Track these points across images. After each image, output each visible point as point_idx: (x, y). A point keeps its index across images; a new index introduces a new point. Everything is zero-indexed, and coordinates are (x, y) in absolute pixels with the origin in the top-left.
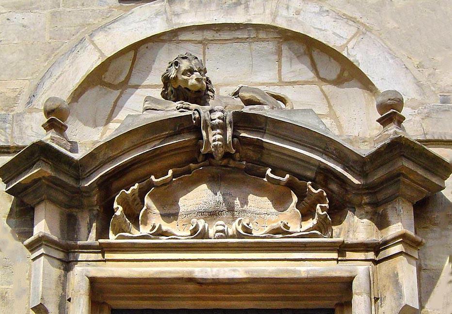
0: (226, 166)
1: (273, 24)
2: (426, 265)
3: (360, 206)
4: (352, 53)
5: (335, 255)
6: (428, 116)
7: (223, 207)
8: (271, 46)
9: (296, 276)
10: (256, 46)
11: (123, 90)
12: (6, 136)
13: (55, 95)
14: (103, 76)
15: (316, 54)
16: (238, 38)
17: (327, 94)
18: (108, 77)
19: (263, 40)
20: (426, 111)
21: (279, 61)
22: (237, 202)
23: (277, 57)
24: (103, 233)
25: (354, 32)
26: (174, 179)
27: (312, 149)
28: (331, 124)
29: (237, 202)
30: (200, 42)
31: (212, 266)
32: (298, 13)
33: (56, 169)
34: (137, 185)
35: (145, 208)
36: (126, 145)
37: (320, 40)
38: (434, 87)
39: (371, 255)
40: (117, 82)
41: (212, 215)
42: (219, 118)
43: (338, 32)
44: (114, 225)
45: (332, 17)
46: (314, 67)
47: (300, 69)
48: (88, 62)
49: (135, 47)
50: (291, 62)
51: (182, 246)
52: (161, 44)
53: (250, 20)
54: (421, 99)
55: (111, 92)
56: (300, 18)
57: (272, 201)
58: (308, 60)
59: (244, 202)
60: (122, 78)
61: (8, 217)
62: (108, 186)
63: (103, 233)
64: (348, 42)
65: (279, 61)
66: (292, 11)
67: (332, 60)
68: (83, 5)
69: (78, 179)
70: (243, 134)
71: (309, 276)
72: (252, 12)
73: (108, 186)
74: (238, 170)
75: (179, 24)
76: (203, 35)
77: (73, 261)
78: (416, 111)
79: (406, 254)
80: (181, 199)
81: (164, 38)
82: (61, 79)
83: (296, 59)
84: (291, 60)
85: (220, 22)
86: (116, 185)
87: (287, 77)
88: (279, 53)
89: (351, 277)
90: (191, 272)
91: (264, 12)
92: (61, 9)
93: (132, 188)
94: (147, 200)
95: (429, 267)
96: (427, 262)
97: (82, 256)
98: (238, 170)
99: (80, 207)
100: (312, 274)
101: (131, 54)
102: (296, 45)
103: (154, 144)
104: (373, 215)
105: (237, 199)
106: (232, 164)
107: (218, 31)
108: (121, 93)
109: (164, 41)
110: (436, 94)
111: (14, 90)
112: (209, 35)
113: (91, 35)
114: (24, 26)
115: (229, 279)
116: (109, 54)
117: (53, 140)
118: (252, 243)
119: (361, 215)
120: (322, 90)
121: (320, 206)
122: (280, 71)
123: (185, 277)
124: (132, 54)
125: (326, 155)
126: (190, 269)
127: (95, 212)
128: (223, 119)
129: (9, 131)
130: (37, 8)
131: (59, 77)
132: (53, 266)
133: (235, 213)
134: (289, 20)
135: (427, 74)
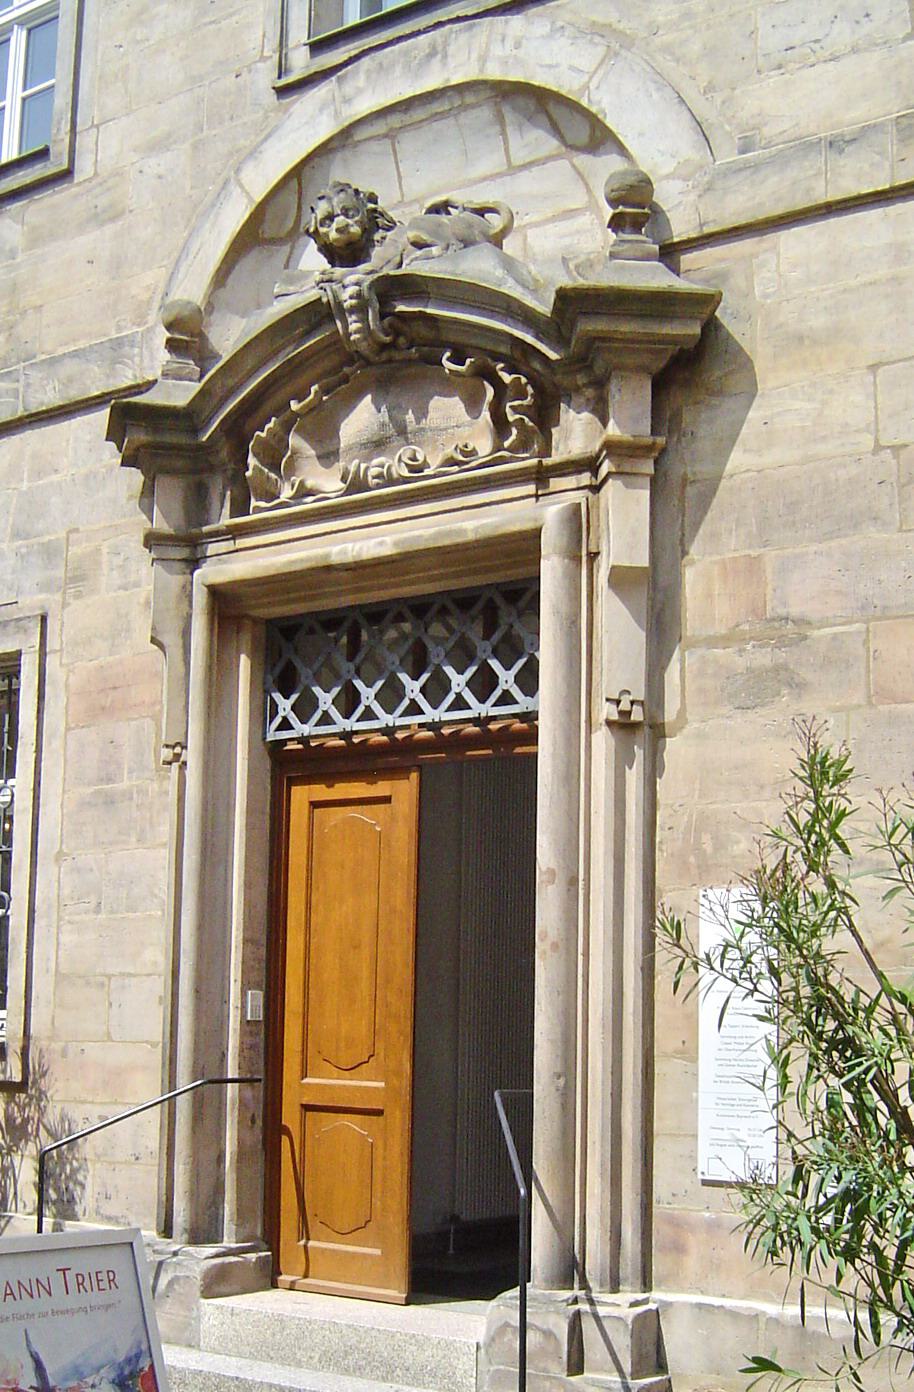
0: (390, 361)
1: (481, 77)
2: (694, 474)
3: (578, 389)
4: (595, 97)
5: (531, 489)
6: (709, 188)
7: (391, 431)
8: (485, 113)
9: (459, 540)
10: (466, 118)
11: (294, 243)
12: (135, 370)
13: (119, 329)
14: (260, 232)
15: (552, 107)
16: (437, 114)
17: (581, 170)
18: (269, 230)
19: (472, 106)
20: (706, 179)
21: (503, 133)
22: (410, 417)
23: (498, 128)
24: (240, 508)
25: (603, 53)
26: (325, 398)
27: (492, 315)
28: (592, 224)
29: (410, 417)
30: (386, 136)
31: (369, 537)
32: (518, 45)
33: (156, 430)
34: (273, 419)
35: (289, 453)
36: (250, 363)
37: (548, 87)
38: (730, 125)
39: (586, 478)
40: (283, 233)
41: (378, 445)
42: (351, 298)
43: (576, 63)
44: (255, 490)
45: (568, 38)
46: (556, 130)
47: (536, 139)
48: (234, 217)
49: (297, 173)
50: (521, 130)
51: (326, 510)
52: (331, 156)
53: (448, 80)
54: (699, 157)
55: (278, 251)
56: (521, 53)
57: (464, 402)
58: (543, 119)
59: (422, 414)
60: (290, 224)
61: (141, 497)
62: (237, 431)
63: (240, 508)
64: (591, 78)
65: (503, 133)
66: (509, 43)
67: (574, 114)
68: (232, 118)
69: (196, 431)
70: (401, 308)
71: (478, 536)
72: (452, 62)
73: (237, 431)
74: (409, 362)
75: (351, 116)
76: (387, 124)
77: (201, 558)
78: (690, 183)
79: (619, 474)
80: (343, 425)
81: (334, 144)
82: (199, 257)
83: (528, 123)
84: (520, 126)
85: (407, 96)
86: (250, 424)
87: (519, 156)
88: (500, 120)
89: (536, 529)
90: (328, 556)
91: (469, 58)
92: (205, 133)
93: (267, 427)
94: (294, 440)
95: (699, 477)
96: (697, 468)
97: (212, 549)
98: (409, 362)
99: (212, 469)
100: (483, 534)
101: (294, 184)
102: (521, 101)
103: (287, 351)
104: (597, 403)
105: (410, 412)
106: (397, 355)
107: (406, 111)
108: (292, 248)
109: (332, 151)
110: (732, 138)
111: (148, 288)
112: (395, 121)
113: (238, 171)
114: (160, 177)
115: (374, 559)
116: (259, 198)
117: (167, 375)
118: (413, 490)
119: (580, 406)
120: (574, 166)
121: (511, 407)
122: (507, 150)
123: (319, 565)
124: (294, 184)
125: (512, 317)
126: (320, 551)
127: (230, 473)
128: (359, 296)
129: (137, 359)
130: (175, 142)
131: (197, 254)
132: (171, 573)
133: (409, 436)
134: (504, 62)
135: (719, 101)
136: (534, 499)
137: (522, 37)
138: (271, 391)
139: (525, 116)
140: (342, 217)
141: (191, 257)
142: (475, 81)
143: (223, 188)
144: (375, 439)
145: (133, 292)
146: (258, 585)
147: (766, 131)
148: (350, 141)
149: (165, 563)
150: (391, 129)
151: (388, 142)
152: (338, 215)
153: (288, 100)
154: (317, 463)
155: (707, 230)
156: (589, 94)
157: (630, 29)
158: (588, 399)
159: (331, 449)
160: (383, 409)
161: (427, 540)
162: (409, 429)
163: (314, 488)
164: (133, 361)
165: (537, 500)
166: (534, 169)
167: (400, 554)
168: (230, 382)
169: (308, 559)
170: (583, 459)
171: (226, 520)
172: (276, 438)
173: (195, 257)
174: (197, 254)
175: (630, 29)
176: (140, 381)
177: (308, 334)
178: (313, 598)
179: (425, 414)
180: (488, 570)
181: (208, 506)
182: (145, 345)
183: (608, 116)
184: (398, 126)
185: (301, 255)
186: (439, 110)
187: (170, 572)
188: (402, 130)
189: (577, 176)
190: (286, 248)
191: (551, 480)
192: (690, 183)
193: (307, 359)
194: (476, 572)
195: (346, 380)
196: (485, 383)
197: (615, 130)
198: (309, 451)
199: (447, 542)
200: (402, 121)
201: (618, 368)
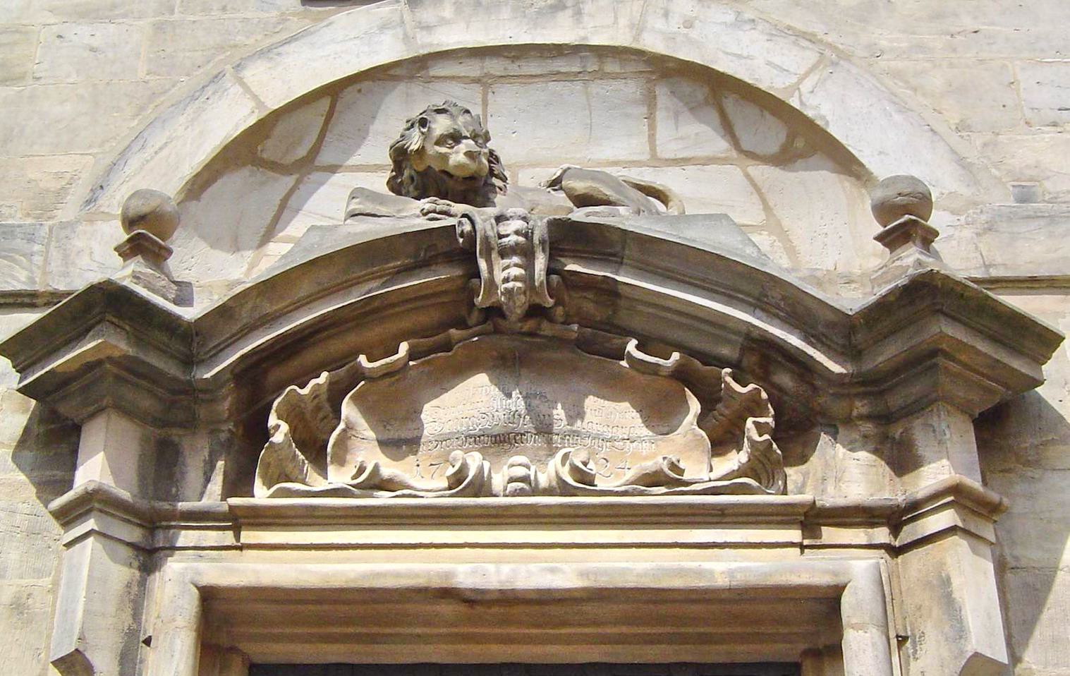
2: (1016, 558)
3: (848, 421)
5: (795, 535)
8: (632, 89)
9: (702, 583)
12: (32, 272)
14: (259, 148)
15: (730, 104)
16: (559, 73)
18: (269, 150)
19: (615, 77)
20: (984, 217)
21: (651, 117)
22: (559, 412)
24: (239, 483)
29: (559, 412)
30: (477, 81)
33: (138, 340)
34: (325, 375)
35: (342, 426)
36: (305, 288)
38: (999, 169)
40: (289, 159)
42: (517, 233)
44: (267, 466)
46: (728, 129)
47: (697, 134)
49: (334, 91)
53: (585, 38)
56: (694, 34)
57: (640, 411)
58: (714, 115)
59: (576, 413)
60: (302, 152)
63: (239, 483)
65: (651, 117)
68: (224, 9)
69: (189, 362)
74: (560, 342)
75: (431, 45)
76: (483, 68)
78: (962, 218)
81: (398, 71)
84: (676, 115)
86: (275, 375)
88: (650, 101)
90: (448, 575)
92: (177, 16)
93: (313, 382)
94: (348, 409)
95: (1023, 563)
97: (186, 538)
99: (190, 424)
100: (740, 580)
101: (325, 104)
102: (686, 87)
105: (559, 406)
106: (547, 329)
107: (514, 59)
108: (298, 182)
112: (495, 66)
113: (238, 67)
114: (93, 50)
117: (138, 278)
120: (747, 176)
121: (754, 422)
124: (325, 104)
127: (223, 436)
129: (38, 259)
130: (125, 16)
131: (161, 149)
133: (555, 437)
134: (671, 38)
135: (979, 143)
136: (798, 550)
137: (696, 18)
138: (319, 336)
139: (686, 104)
140: (471, 142)
141: (150, 151)
142: (625, 48)
143: (212, 81)
144: (496, 431)
145: (32, 176)
146: (979, 514)
147: (1048, 185)
148: (423, 73)
149: (108, 542)
150: (486, 75)
151: (477, 88)
152: (466, 138)
153: (319, 9)
154: (378, 449)
155: (994, 273)
156: (800, 96)
157: (842, 44)
158: (865, 437)
159: (405, 434)
160: (515, 394)
161: (638, 575)
162: (556, 428)
163: (397, 479)
164: (31, 261)
165: (802, 553)
166: (691, 169)
167: (584, 589)
168: (268, 308)
169: (408, 575)
170: (881, 508)
171: (213, 497)
172: (316, 401)
173: (156, 153)
174: (161, 149)
175: (842, 44)
176: (39, 288)
177: (407, 271)
178: (373, 639)
179: (580, 415)
180: (704, 639)
181: (178, 476)
182: (53, 244)
183: (831, 123)
184: (498, 74)
185: (311, 194)
186: (563, 70)
187: (114, 559)
188: (502, 80)
189: (751, 189)
190: (289, 181)
191: (824, 528)
192: (962, 218)
193: (393, 305)
194: (684, 639)
195: (447, 347)
196: (686, 389)
197: (843, 141)
198: (365, 429)
199: (678, 583)
200: (505, 69)
201: (948, 400)
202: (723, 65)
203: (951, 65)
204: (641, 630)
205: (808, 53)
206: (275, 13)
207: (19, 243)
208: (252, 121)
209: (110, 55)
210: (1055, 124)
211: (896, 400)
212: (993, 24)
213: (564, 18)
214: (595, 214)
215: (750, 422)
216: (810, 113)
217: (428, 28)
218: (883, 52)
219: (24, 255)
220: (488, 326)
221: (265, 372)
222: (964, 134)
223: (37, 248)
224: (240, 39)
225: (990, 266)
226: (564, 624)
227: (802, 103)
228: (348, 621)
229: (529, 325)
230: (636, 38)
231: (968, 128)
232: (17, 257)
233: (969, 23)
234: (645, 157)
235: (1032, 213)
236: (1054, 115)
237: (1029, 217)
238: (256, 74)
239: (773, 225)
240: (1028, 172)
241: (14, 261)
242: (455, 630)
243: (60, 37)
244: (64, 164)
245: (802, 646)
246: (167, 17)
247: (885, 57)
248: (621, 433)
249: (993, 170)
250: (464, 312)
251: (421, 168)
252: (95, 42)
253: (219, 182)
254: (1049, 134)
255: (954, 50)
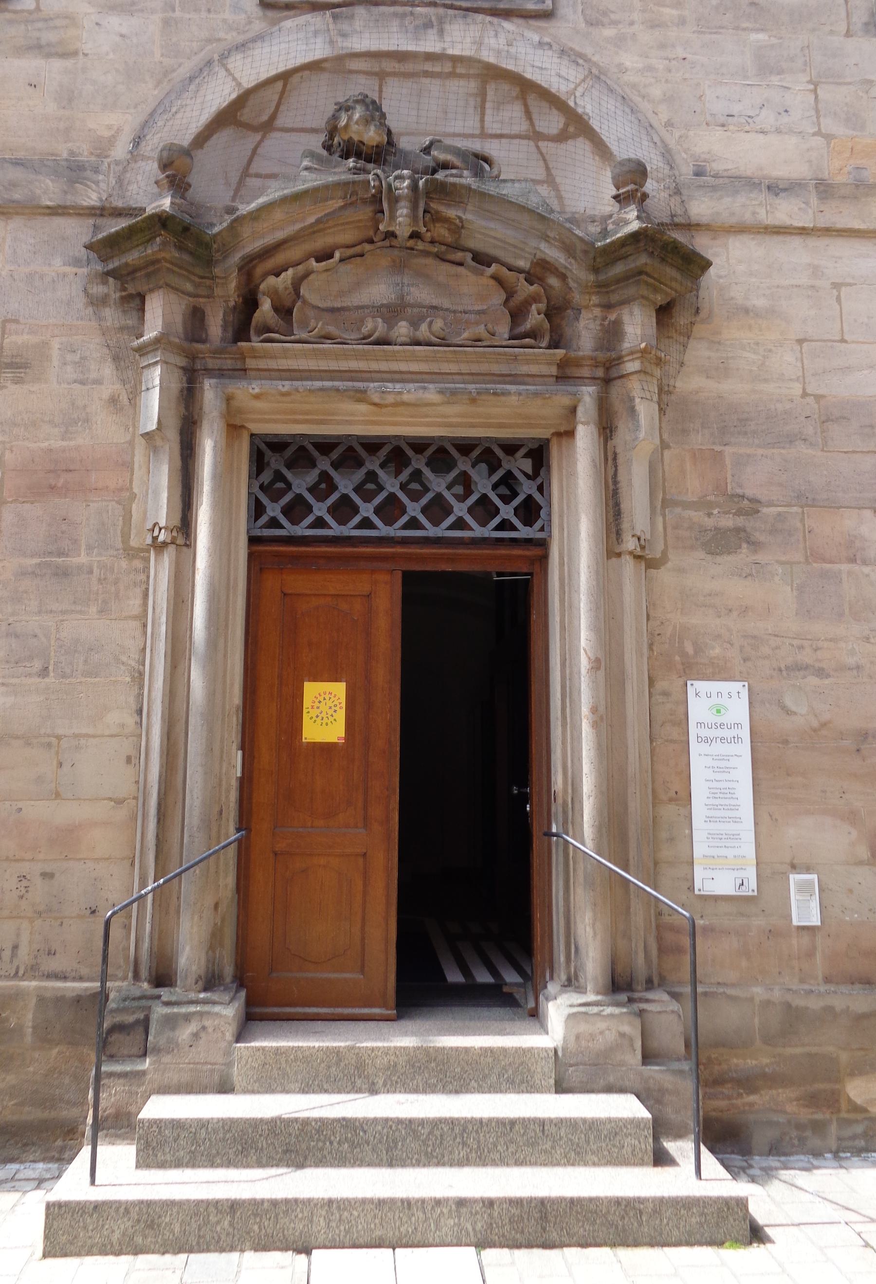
12: (100, 193)
14: (239, 114)
18: (246, 115)
49: (285, 77)
56: (513, 50)
60: (265, 118)
92: (178, 14)
101: (279, 85)
106: (420, 246)
112: (389, 66)
114: (122, 36)
120: (538, 147)
124: (279, 85)
130: (142, 11)
147: (715, 166)
190: (258, 137)
202: (529, 74)
203: (667, 81)
204: (465, 420)
205: (580, 69)
206: (243, 16)
207: (88, 173)
208: (234, 96)
209: (135, 41)
210: (723, 125)
211: (615, 298)
212: (695, 54)
213: (432, 34)
214: (452, 175)
215: (534, 307)
216: (580, 110)
217: (344, 35)
218: (627, 70)
219: (93, 182)
220: (387, 243)
221: (254, 267)
222: (669, 128)
223: (101, 177)
224: (222, 35)
225: (675, 216)
226: (427, 416)
227: (575, 103)
228: (307, 413)
229: (411, 243)
230: (479, 49)
231: (672, 125)
232: (89, 183)
233: (680, 52)
234: (477, 132)
235: (702, 184)
236: (723, 119)
237: (700, 186)
238: (236, 62)
239: (550, 180)
240: (703, 156)
241: (86, 185)
242: (367, 418)
243: (97, 24)
244: (113, 119)
245: (552, 431)
246: (171, 14)
247: (628, 73)
248: (460, 308)
249: (683, 154)
250: (371, 233)
251: (346, 138)
252: (124, 31)
253: (215, 137)
254: (719, 132)
255: (670, 71)
